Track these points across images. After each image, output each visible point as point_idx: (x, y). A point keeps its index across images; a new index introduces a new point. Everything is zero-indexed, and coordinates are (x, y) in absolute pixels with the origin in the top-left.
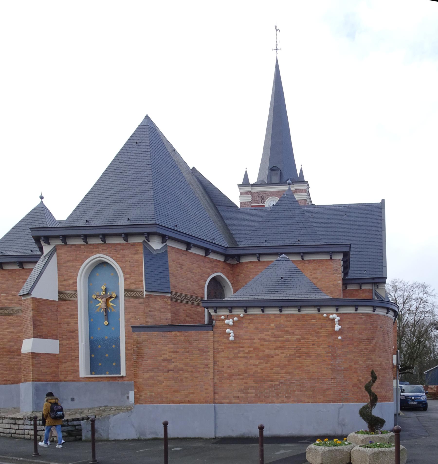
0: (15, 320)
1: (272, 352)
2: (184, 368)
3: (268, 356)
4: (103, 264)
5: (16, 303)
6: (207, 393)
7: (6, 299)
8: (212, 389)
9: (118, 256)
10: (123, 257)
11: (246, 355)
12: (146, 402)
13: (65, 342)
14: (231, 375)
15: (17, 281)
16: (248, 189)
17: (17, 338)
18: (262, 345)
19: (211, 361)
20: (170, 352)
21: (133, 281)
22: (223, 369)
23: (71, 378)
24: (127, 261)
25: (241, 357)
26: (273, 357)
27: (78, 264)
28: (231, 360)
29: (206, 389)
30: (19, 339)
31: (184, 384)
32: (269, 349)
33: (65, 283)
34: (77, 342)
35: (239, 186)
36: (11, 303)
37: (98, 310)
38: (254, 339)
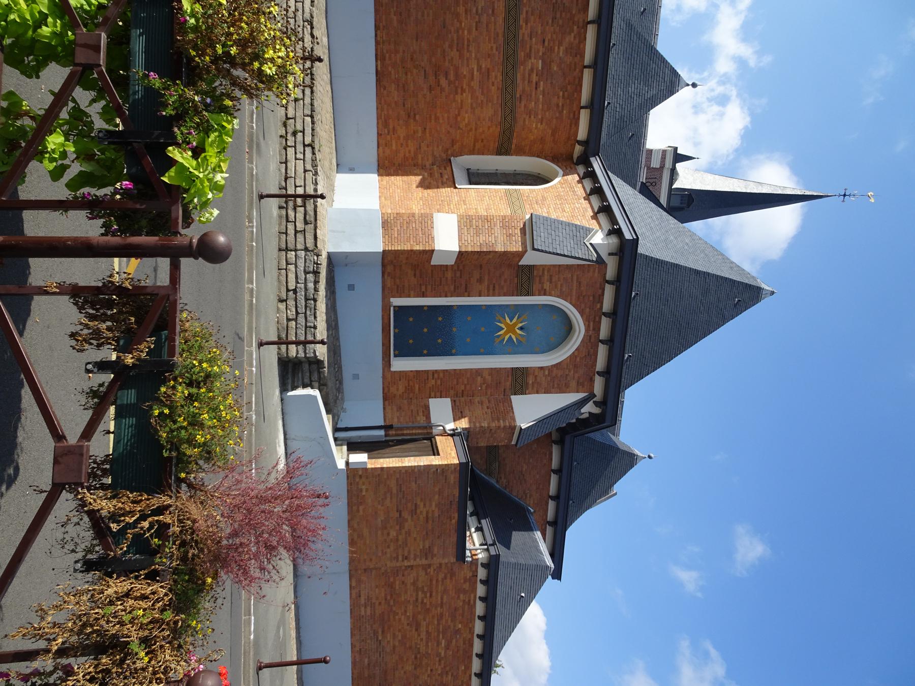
0: (493, 83)
1: (423, 629)
2: (403, 531)
3: (418, 626)
4: (569, 328)
5: (523, 91)
6: (365, 561)
7: (532, 70)
8: (372, 566)
9: (578, 359)
10: (575, 366)
11: (420, 600)
12: (351, 484)
13: (449, 275)
14: (391, 586)
15: (561, 93)
16: (668, 164)
17: (462, 88)
18: (433, 617)
19: (412, 563)
20: (427, 512)
21: (538, 380)
22: (400, 576)
23: (389, 284)
24: (570, 371)
25: (417, 595)
26: (417, 630)
27: (574, 297)
28: (414, 584)
29: (371, 560)
30: (459, 90)
31: (379, 532)
32: (427, 627)
33: (546, 277)
34: (449, 294)
35: (676, 149)
36: (523, 79)
37: (499, 317)
38: (442, 607)
